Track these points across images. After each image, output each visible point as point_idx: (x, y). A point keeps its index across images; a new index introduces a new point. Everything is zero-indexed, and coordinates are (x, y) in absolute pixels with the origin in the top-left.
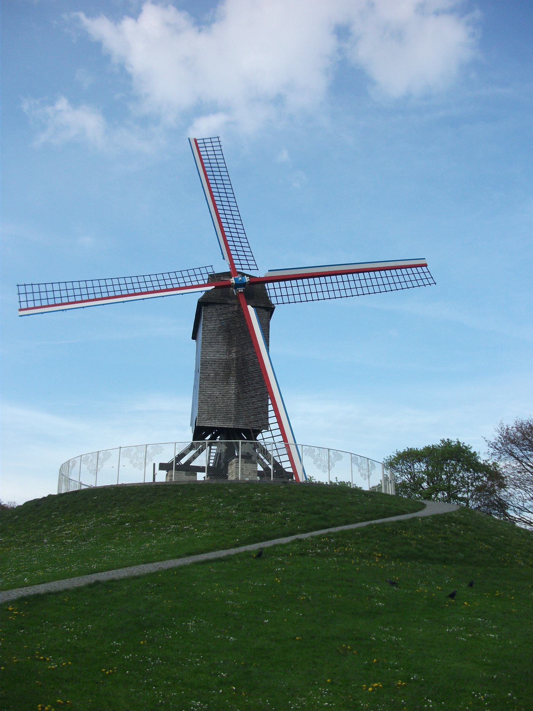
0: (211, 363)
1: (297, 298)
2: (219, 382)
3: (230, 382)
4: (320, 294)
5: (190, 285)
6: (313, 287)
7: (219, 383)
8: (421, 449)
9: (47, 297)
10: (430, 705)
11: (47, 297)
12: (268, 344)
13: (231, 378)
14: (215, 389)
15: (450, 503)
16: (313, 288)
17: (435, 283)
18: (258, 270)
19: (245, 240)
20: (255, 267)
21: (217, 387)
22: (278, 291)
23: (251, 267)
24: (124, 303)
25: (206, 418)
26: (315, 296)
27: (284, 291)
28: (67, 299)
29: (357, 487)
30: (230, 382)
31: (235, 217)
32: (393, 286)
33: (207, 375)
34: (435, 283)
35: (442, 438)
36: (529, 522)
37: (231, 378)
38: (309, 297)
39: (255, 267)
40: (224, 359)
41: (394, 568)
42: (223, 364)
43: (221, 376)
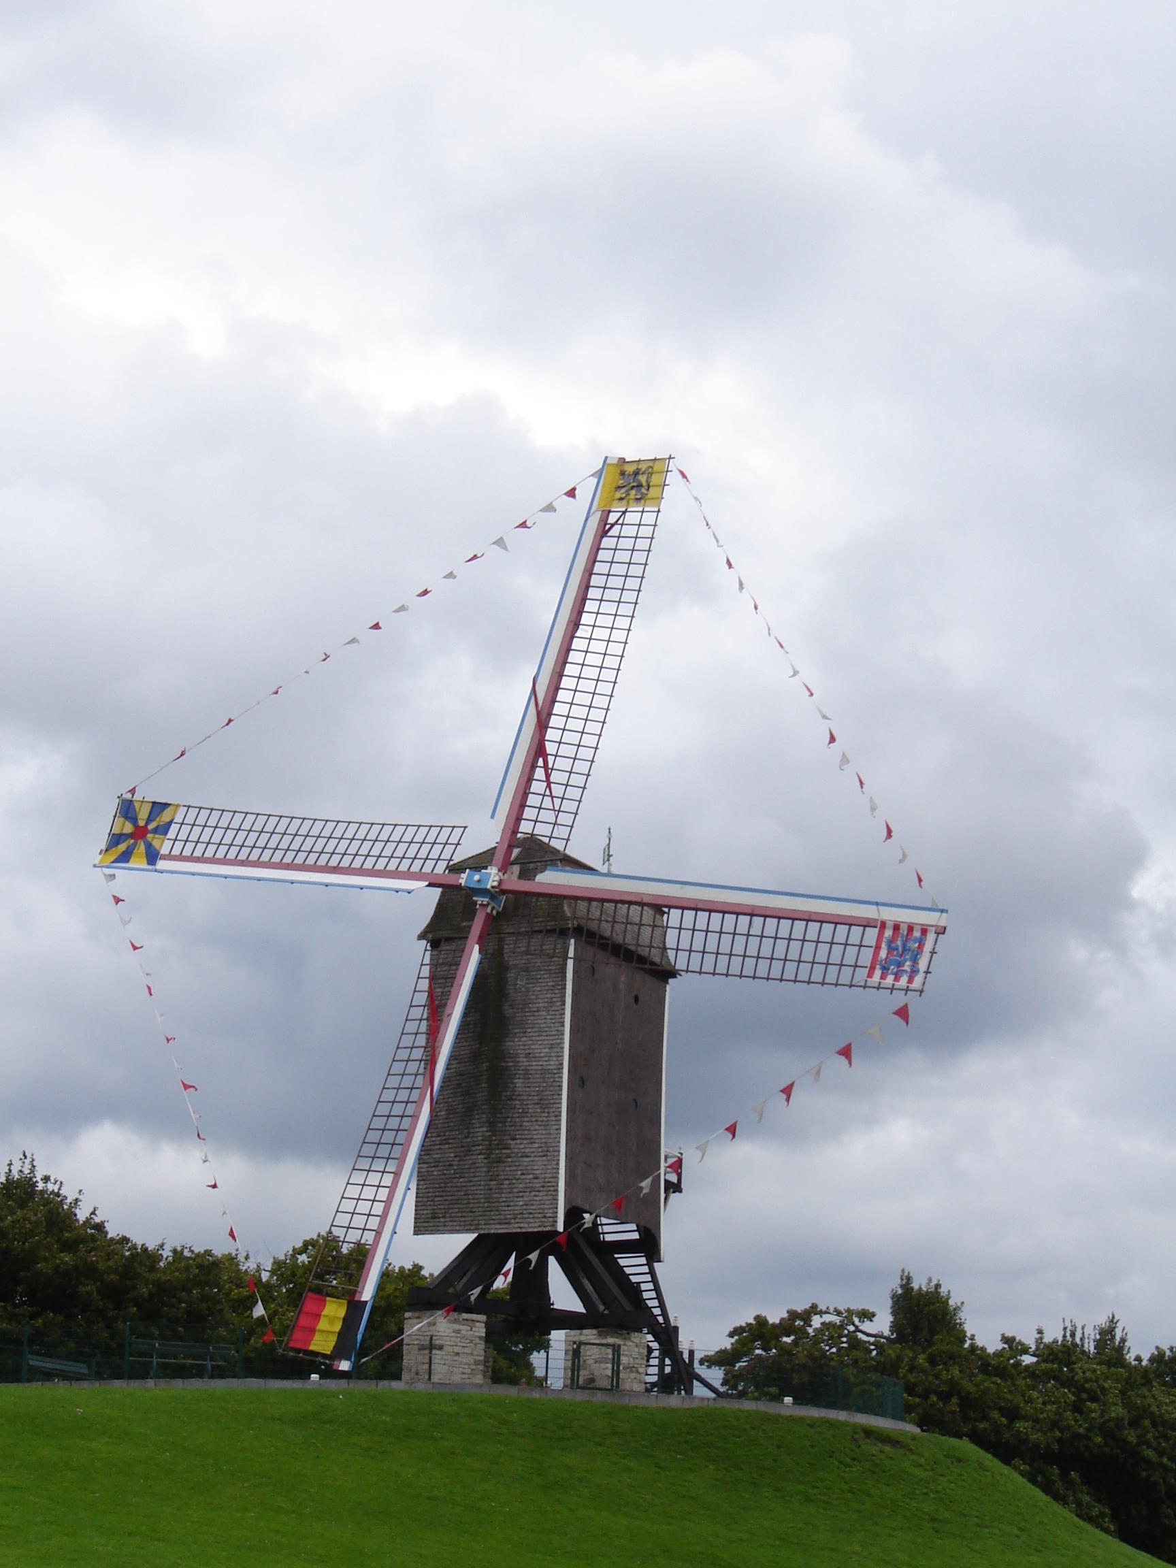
1: (593, 727)
4: (586, 740)
5: (426, 996)
6: (575, 711)
9: (681, 950)
11: (681, 950)
16: (593, 659)
17: (670, 458)
18: (465, 827)
19: (365, 828)
20: (458, 832)
22: (591, 659)
23: (454, 840)
24: (409, 1189)
26: (611, 662)
27: (593, 659)
28: (810, 943)
31: (281, 829)
32: (641, 544)
34: (670, 458)
36: (586, 1282)
38: (611, 662)
39: (458, 832)
41: (668, 1361)
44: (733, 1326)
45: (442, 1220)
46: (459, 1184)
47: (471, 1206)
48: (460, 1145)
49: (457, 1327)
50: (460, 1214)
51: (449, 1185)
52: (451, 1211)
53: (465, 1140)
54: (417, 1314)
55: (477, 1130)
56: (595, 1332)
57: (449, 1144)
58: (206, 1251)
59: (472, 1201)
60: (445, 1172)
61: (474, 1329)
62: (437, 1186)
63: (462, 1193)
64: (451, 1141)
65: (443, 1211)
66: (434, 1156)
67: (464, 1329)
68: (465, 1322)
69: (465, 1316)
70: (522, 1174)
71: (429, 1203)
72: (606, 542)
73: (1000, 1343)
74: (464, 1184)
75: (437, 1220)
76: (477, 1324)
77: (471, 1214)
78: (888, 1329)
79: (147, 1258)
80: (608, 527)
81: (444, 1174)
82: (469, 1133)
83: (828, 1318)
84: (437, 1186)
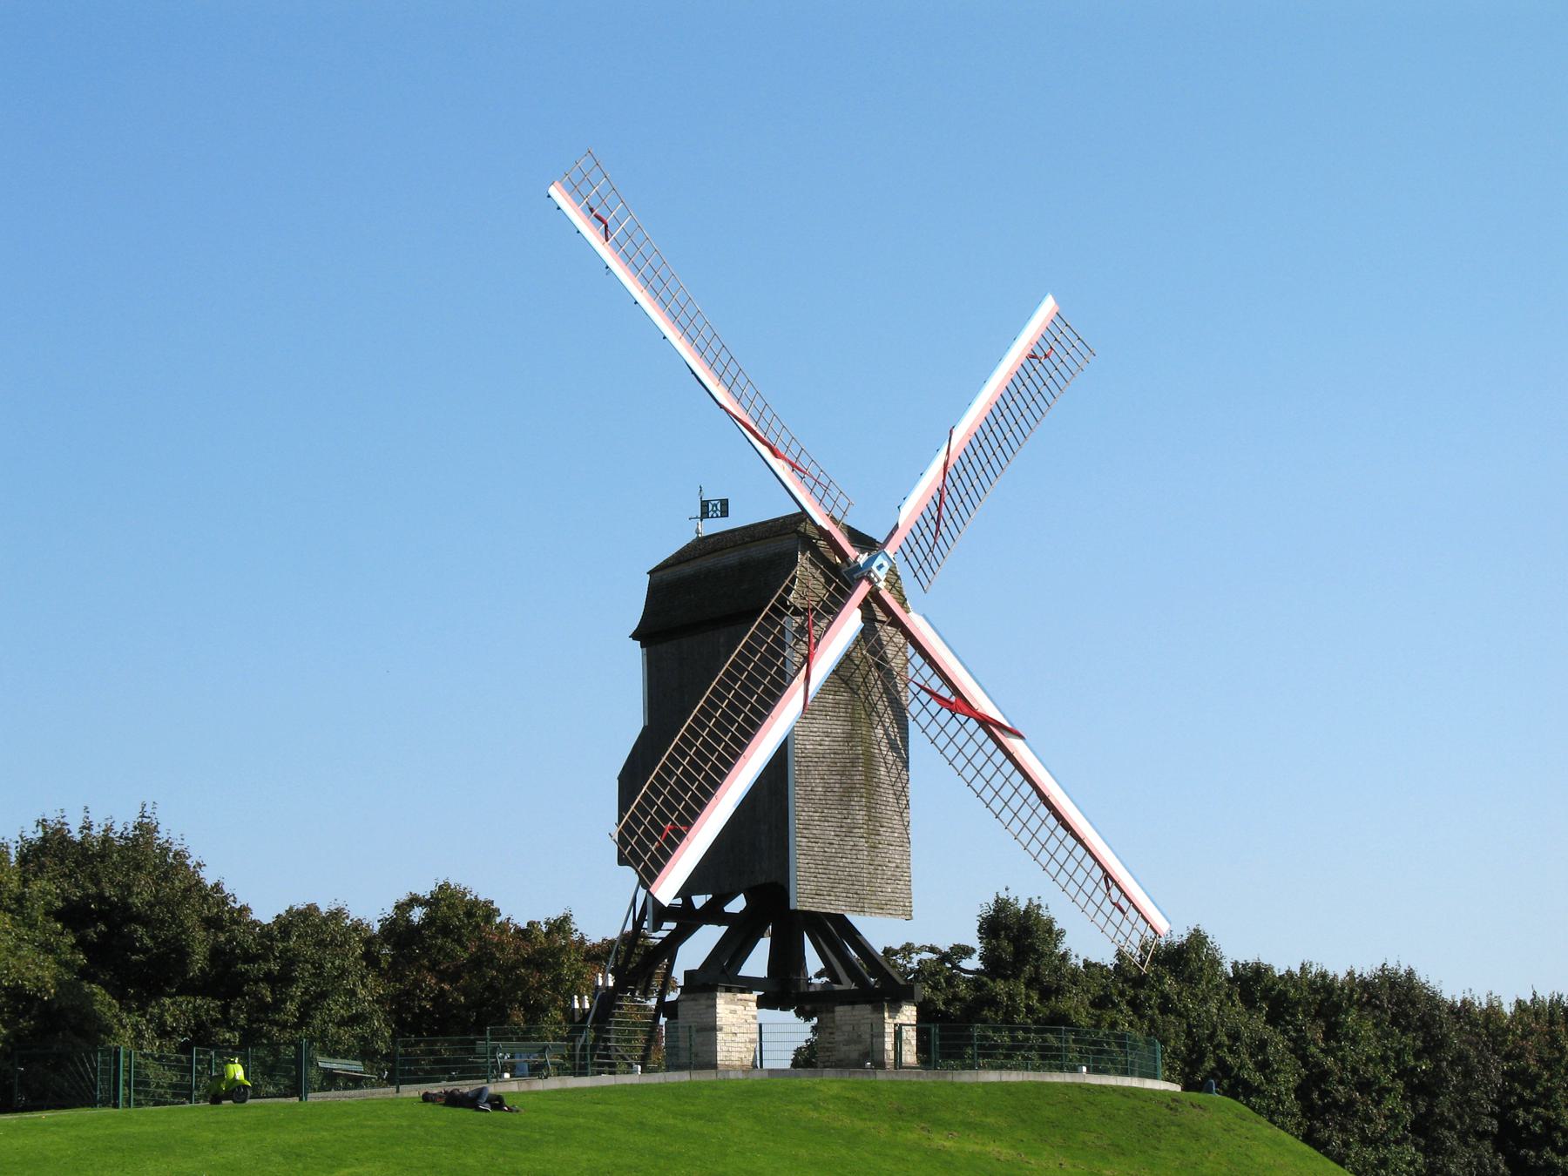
0: (816, 760)
2: (833, 807)
3: (854, 808)
7: (833, 811)
8: (87, 827)
10: (507, 1072)
12: (905, 735)
13: (856, 799)
14: (826, 824)
15: (1085, 961)
21: (830, 819)
25: (814, 892)
29: (763, 937)
30: (854, 808)
33: (810, 789)
35: (132, 818)
37: (856, 799)
40: (840, 752)
42: (838, 764)
43: (837, 794)
44: (1400, 958)
45: (827, 898)
46: (841, 864)
47: (857, 887)
48: (839, 824)
49: (733, 1007)
50: (844, 895)
51: (832, 863)
52: (835, 890)
53: (845, 821)
54: (693, 996)
55: (857, 812)
56: (869, 1007)
57: (828, 821)
58: (309, 907)
59: (856, 883)
60: (826, 849)
61: (747, 1008)
62: (819, 862)
63: (846, 874)
64: (830, 819)
65: (828, 889)
66: (815, 832)
67: (739, 1008)
68: (739, 1002)
69: (740, 996)
70: (889, 862)
71: (812, 879)
72: (1098, 873)
73: (498, 907)
74: (847, 865)
75: (822, 897)
76: (750, 1004)
77: (855, 896)
78: (257, 919)
79: (1433, 1000)
80: (1110, 883)
81: (825, 852)
82: (849, 814)
83: (926, 956)
84: (819, 862)
